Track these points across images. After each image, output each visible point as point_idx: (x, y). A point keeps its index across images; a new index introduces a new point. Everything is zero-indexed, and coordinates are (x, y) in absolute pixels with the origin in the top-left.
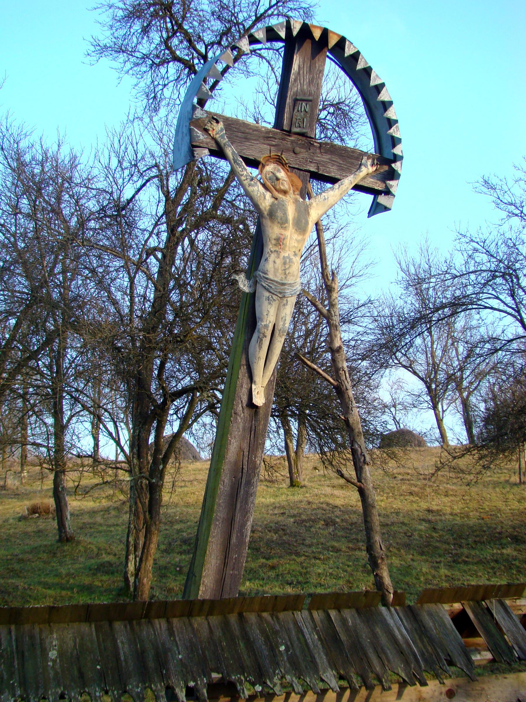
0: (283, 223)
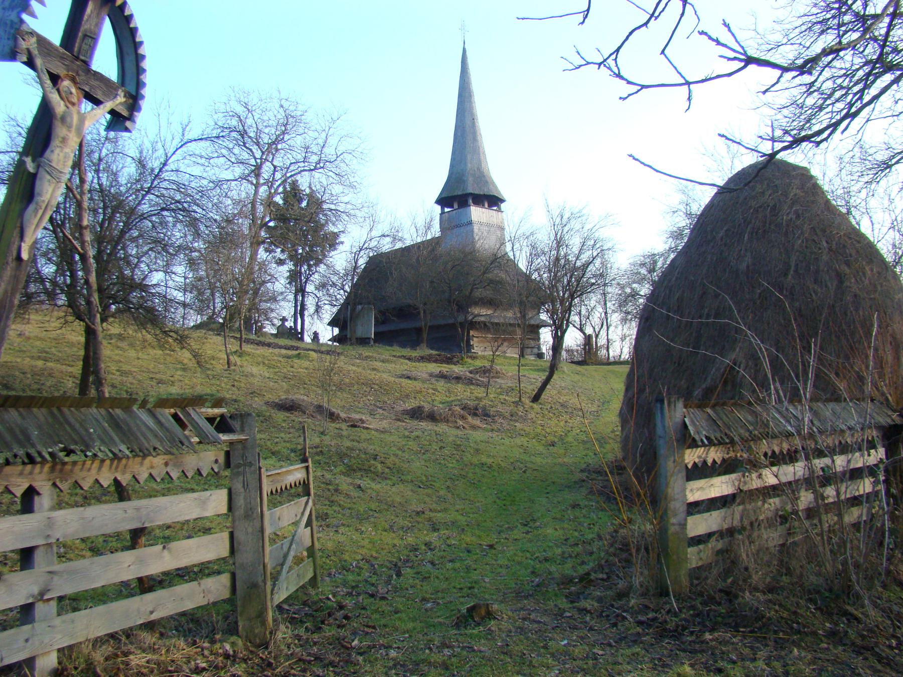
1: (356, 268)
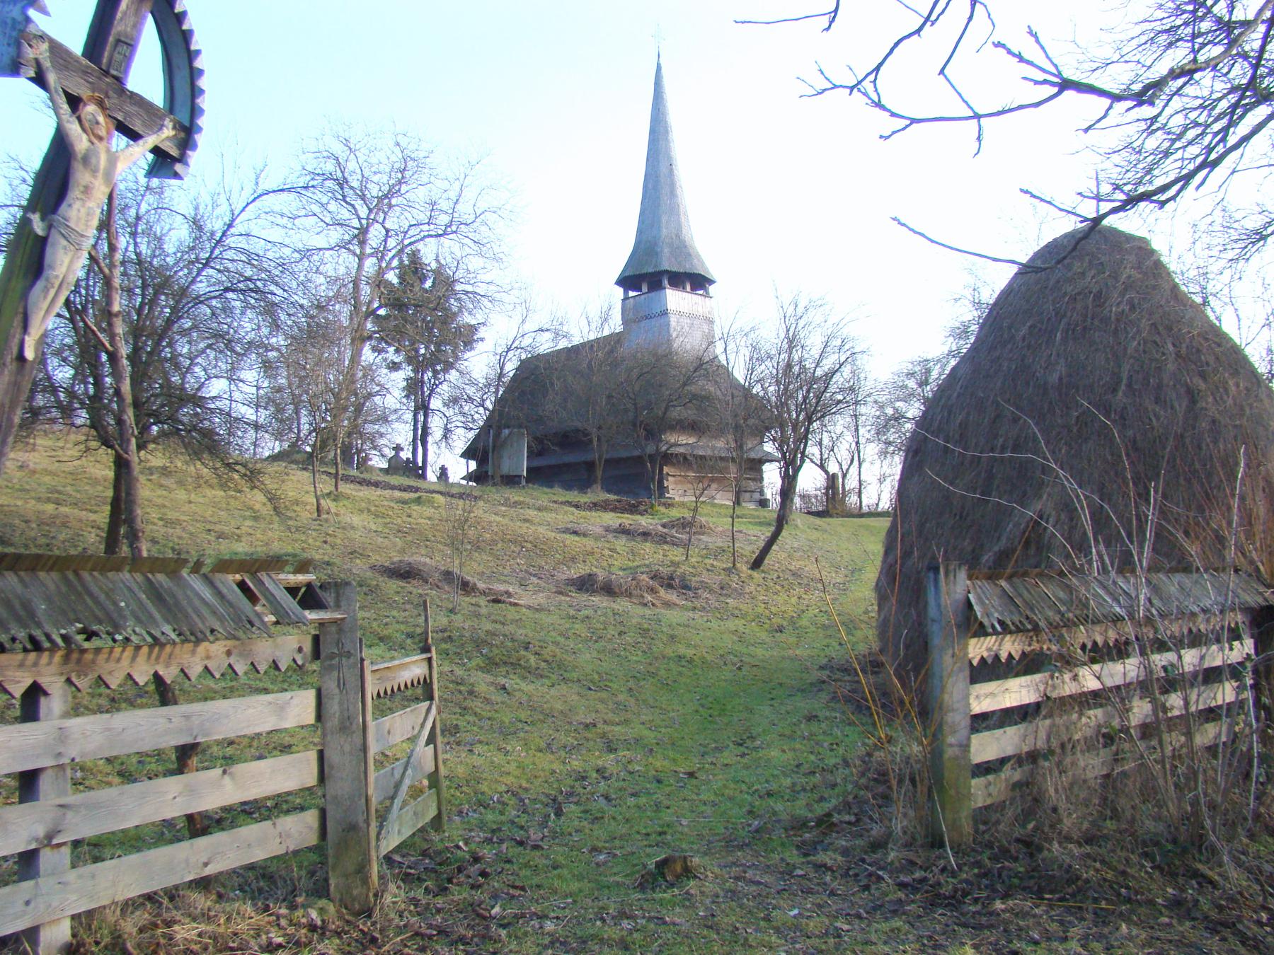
0: (95, 171)
1: (501, 375)
